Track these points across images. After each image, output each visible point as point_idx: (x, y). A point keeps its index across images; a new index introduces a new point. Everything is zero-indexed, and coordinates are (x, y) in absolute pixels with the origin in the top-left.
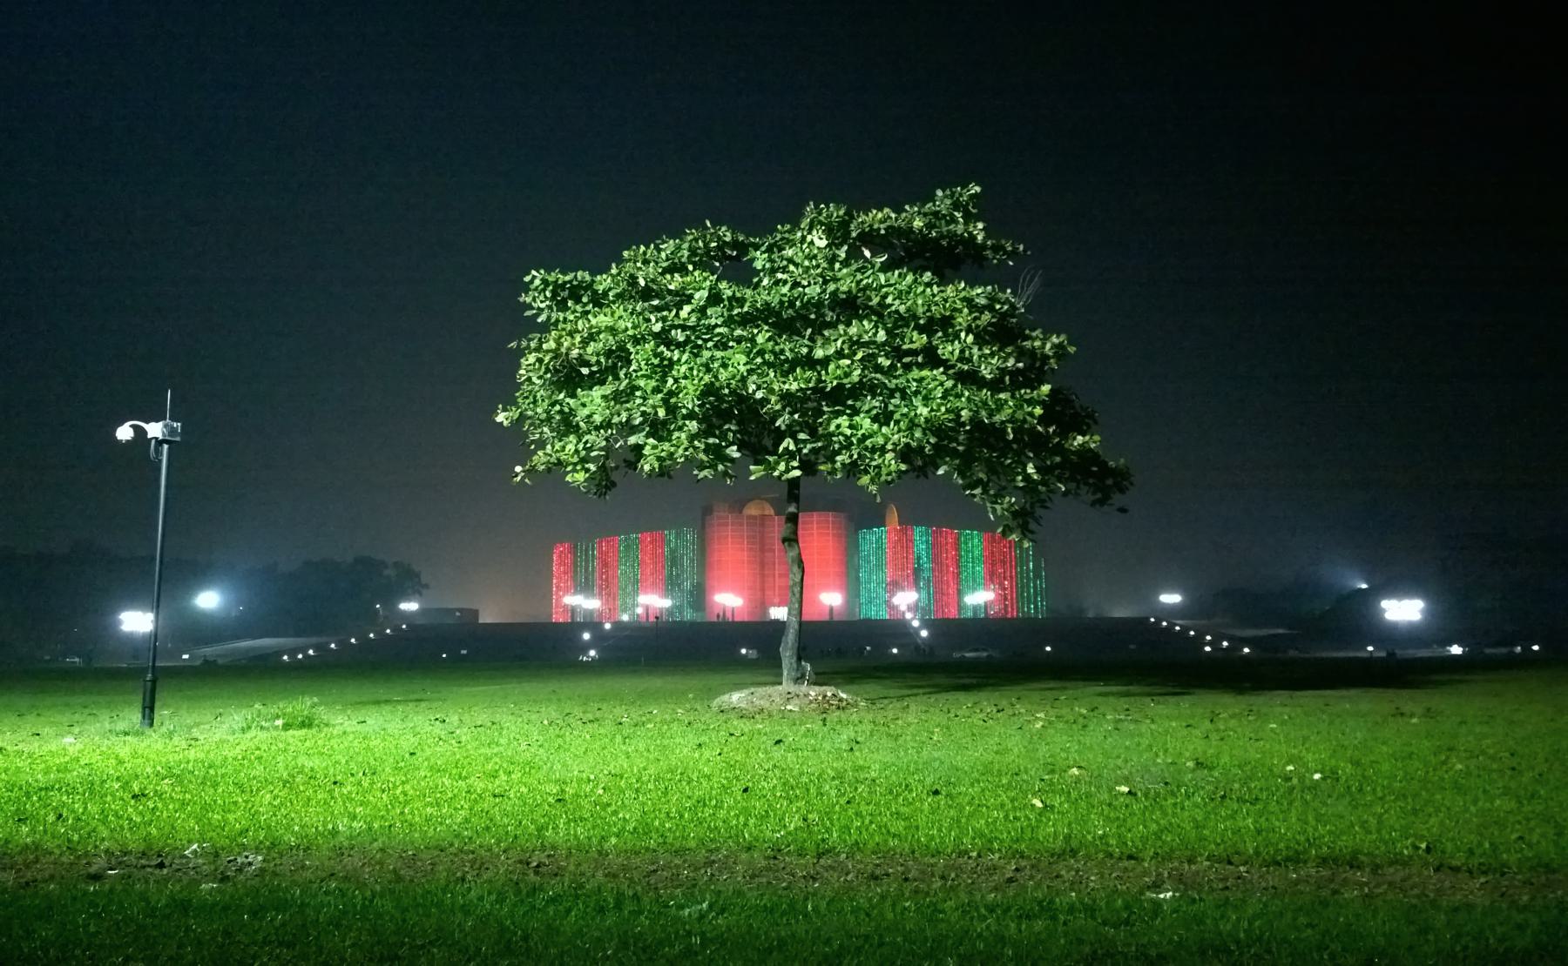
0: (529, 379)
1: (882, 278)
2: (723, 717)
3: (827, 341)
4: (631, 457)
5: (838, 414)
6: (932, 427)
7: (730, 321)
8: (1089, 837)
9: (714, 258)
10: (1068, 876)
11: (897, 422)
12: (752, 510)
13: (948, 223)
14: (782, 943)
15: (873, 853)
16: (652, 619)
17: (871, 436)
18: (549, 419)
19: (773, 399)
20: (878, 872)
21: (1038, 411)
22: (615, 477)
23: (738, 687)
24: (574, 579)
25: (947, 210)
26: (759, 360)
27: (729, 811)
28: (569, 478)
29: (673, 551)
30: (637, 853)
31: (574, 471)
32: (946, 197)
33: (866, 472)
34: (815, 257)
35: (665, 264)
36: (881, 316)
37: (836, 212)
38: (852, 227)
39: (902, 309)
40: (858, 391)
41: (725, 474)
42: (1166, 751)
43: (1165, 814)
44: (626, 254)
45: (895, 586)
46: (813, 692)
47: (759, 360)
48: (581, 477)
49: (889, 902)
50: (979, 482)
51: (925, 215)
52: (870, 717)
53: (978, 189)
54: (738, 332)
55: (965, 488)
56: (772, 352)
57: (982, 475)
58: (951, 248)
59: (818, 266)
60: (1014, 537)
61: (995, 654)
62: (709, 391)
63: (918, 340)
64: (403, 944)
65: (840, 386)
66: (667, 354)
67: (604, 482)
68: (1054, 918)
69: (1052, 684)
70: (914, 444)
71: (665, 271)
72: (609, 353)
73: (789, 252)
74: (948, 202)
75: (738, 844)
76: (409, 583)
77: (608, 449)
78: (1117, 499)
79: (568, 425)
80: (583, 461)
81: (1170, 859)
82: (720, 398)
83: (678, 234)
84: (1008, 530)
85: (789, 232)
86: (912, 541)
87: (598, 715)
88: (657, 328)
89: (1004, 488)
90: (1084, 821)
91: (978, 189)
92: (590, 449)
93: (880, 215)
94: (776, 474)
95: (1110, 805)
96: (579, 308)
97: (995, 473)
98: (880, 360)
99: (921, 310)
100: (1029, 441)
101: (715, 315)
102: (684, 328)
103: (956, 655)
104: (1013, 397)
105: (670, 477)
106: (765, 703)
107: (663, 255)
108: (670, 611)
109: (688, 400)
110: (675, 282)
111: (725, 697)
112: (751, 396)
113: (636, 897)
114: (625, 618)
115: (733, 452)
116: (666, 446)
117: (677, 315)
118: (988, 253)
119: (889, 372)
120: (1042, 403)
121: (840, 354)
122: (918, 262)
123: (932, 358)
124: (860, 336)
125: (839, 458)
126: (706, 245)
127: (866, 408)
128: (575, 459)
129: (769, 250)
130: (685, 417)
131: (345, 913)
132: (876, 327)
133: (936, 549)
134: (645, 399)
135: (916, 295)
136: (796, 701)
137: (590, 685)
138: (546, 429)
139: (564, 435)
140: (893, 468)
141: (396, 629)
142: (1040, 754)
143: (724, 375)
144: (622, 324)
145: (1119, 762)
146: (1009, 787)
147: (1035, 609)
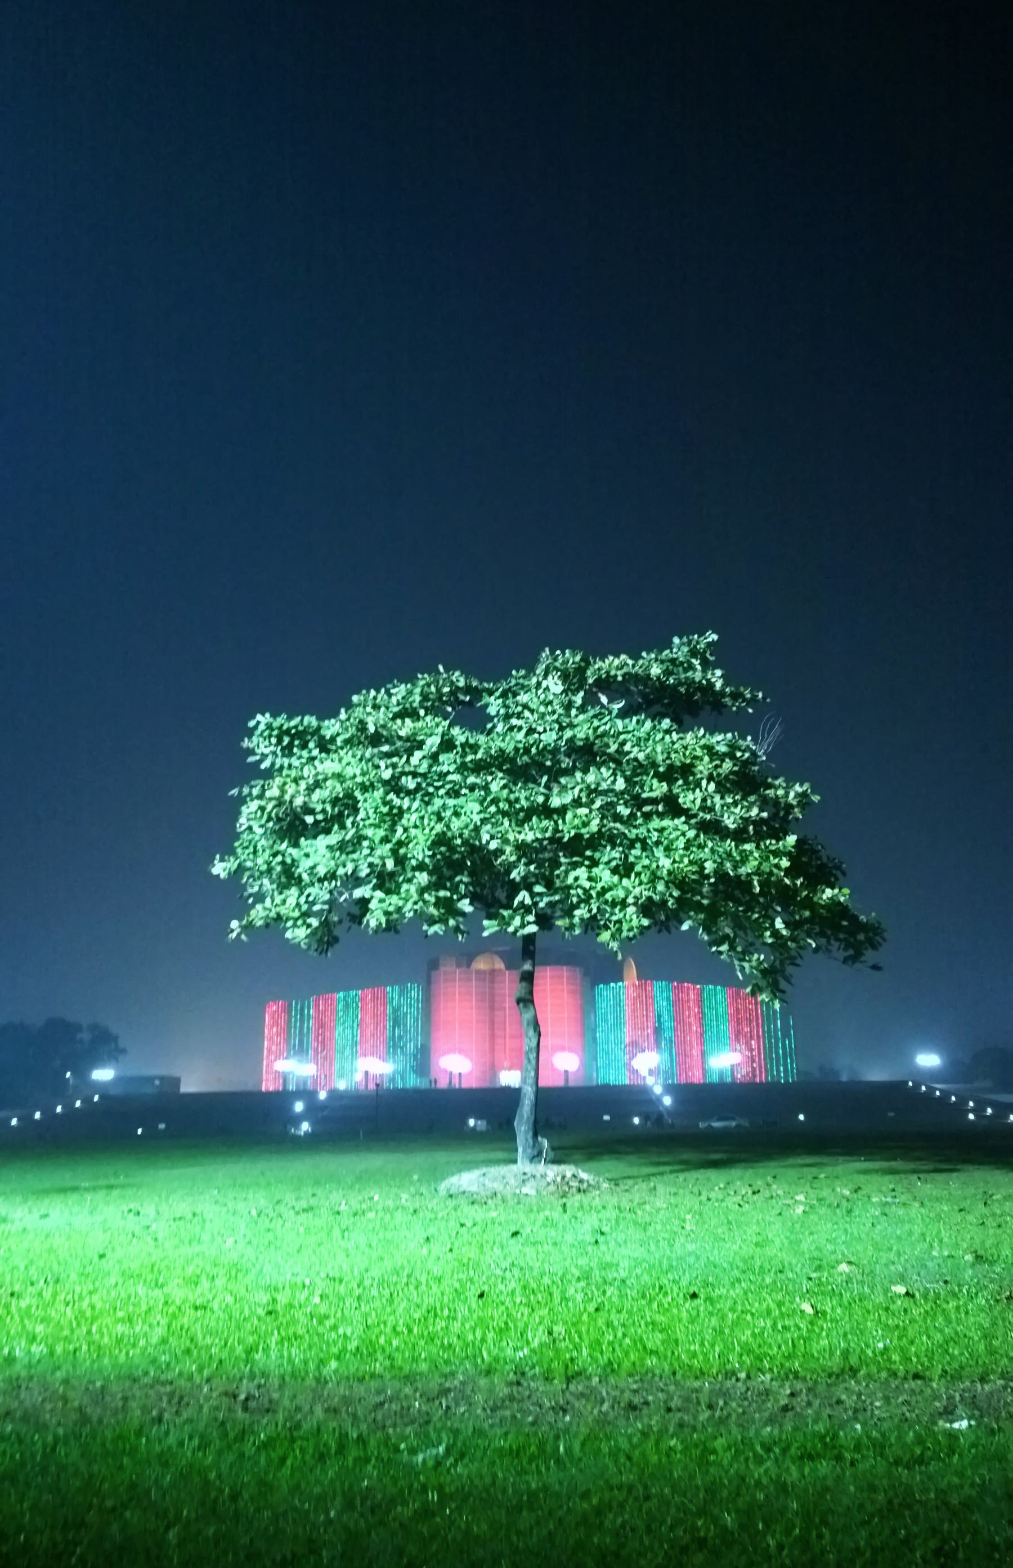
0: (250, 828)
1: (620, 723)
2: (451, 1204)
3: (564, 789)
4: (356, 911)
5: (575, 866)
6: (677, 880)
8: (869, 1352)
9: (446, 703)
10: (849, 1401)
11: (638, 874)
12: (481, 964)
13: (686, 670)
14: (533, 1495)
15: (631, 1375)
16: (372, 1086)
17: (610, 889)
18: (270, 870)
19: (508, 849)
20: (637, 1400)
21: (785, 863)
22: (337, 932)
23: (469, 1165)
24: (287, 1040)
25: (683, 656)
27: (462, 1326)
28: (288, 935)
29: (395, 1010)
30: (361, 1380)
31: (295, 926)
32: (683, 644)
33: (606, 927)
34: (551, 703)
35: (396, 709)
36: (618, 763)
37: (572, 658)
38: (589, 673)
39: (641, 756)
40: (596, 842)
41: (457, 929)
43: (948, 1321)
44: (355, 698)
45: (635, 1047)
46: (553, 1171)
47: (493, 809)
49: (651, 1443)
50: (725, 938)
51: (662, 662)
52: (615, 1200)
53: (715, 637)
54: (472, 779)
55: (711, 944)
56: (507, 800)
57: (728, 930)
58: (689, 695)
59: (554, 712)
60: (764, 997)
61: (745, 1123)
62: (441, 841)
63: (659, 789)
64: (90, 1506)
65: (578, 836)
66: (397, 802)
67: (326, 938)
68: (839, 1458)
69: (809, 1160)
70: (656, 898)
71: (396, 716)
72: (335, 801)
73: (523, 698)
74: (686, 649)
75: (476, 1365)
76: (104, 1045)
77: (332, 903)
79: (289, 877)
80: (306, 915)
81: (960, 1378)
82: (452, 849)
83: (412, 679)
84: (757, 990)
85: (524, 677)
86: (653, 998)
87: (313, 1202)
88: (387, 775)
89: (752, 944)
90: (860, 1331)
91: (715, 637)
92: (313, 903)
93: (617, 662)
94: (511, 929)
95: (887, 1309)
101: (448, 762)
102: (415, 775)
104: (758, 847)
105: (397, 932)
106: (498, 1186)
107: (394, 700)
109: (419, 851)
110: (406, 728)
111: (454, 1180)
112: (482, 848)
113: (361, 1440)
114: (341, 1085)
115: (465, 905)
116: (394, 899)
117: (408, 761)
118: (727, 700)
119: (629, 821)
120: (789, 855)
121: (577, 803)
122: (657, 708)
123: (673, 808)
124: (598, 784)
125: (577, 913)
127: (605, 859)
129: (504, 695)
130: (414, 869)
131: (23, 1464)
132: (614, 774)
133: (678, 1005)
137: (303, 1165)
139: (279, 880)
140: (635, 923)
141: (87, 1101)
142: (804, 1246)
143: (456, 824)
145: (892, 1256)
146: (773, 1288)
147: (785, 1072)
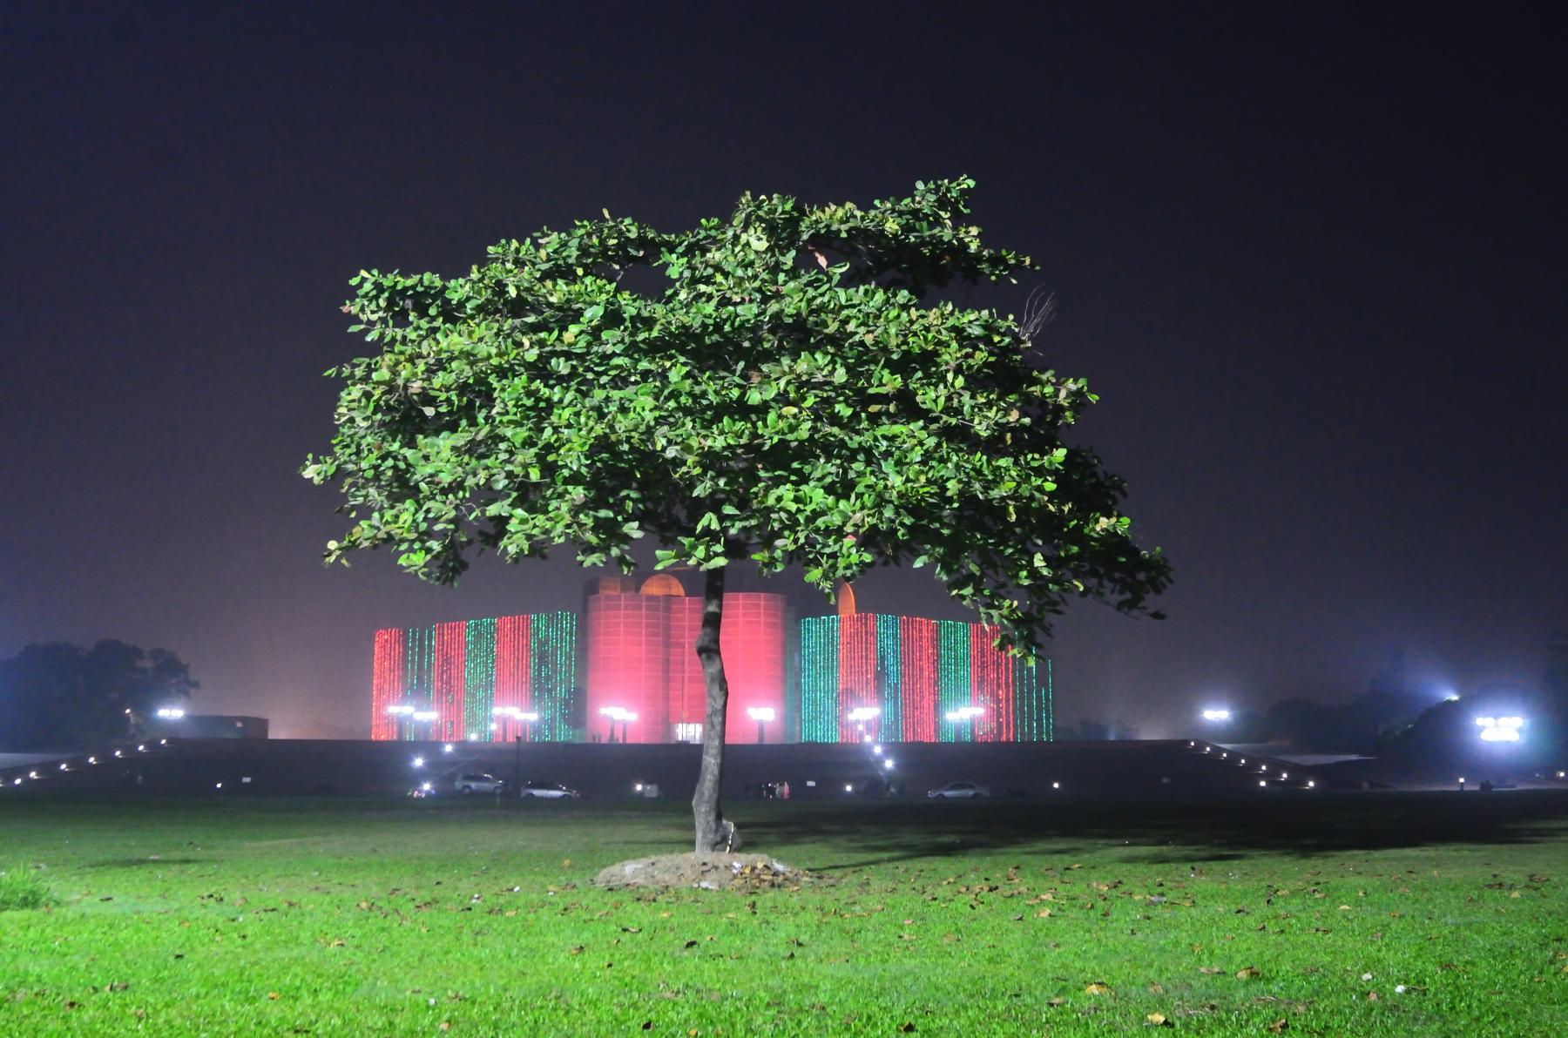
0: (352, 420)
1: (842, 295)
2: (612, 898)
4: (491, 530)
5: (778, 482)
7: (631, 350)
9: (611, 259)
11: (860, 496)
13: (931, 226)
17: (823, 513)
19: (691, 460)
21: (1050, 486)
22: (465, 555)
26: (672, 404)
28: (402, 561)
31: (411, 550)
32: (929, 191)
33: (818, 564)
34: (751, 264)
37: (782, 206)
39: (869, 339)
40: (806, 451)
41: (621, 560)
42: (1211, 953)
45: (848, 696)
46: (738, 862)
48: (419, 559)
50: (969, 579)
51: (901, 214)
53: (971, 183)
54: (644, 365)
57: (974, 568)
58: (935, 258)
59: (755, 277)
60: (1015, 652)
61: (985, 792)
65: (783, 443)
66: (545, 392)
67: (451, 564)
71: (546, 275)
72: (463, 388)
73: (715, 256)
74: (932, 198)
76: (171, 675)
78: (1151, 601)
79: (403, 487)
82: (618, 456)
83: (565, 226)
85: (715, 228)
87: (438, 892)
88: (532, 355)
89: (1003, 585)
91: (971, 183)
92: (436, 520)
94: (692, 562)
96: (424, 323)
97: (994, 566)
98: (838, 407)
99: (893, 342)
100: (1040, 524)
102: (568, 355)
103: (930, 794)
104: (1016, 463)
105: (544, 557)
106: (669, 878)
107: (543, 254)
108: (537, 730)
109: (573, 459)
111: (616, 869)
114: (473, 737)
115: (633, 529)
116: (540, 519)
117: (559, 338)
121: (783, 399)
122: (891, 274)
123: (908, 407)
124: (811, 375)
125: (779, 543)
126: (602, 242)
127: (817, 474)
128: (413, 536)
129: (689, 252)
130: (566, 481)
132: (833, 362)
134: (511, 453)
135: (888, 321)
136: (713, 875)
138: (372, 491)
139: (397, 492)
140: (854, 559)
142: (1048, 963)
143: (623, 424)
144: (482, 350)
145: (1152, 974)
147: (1042, 731)
